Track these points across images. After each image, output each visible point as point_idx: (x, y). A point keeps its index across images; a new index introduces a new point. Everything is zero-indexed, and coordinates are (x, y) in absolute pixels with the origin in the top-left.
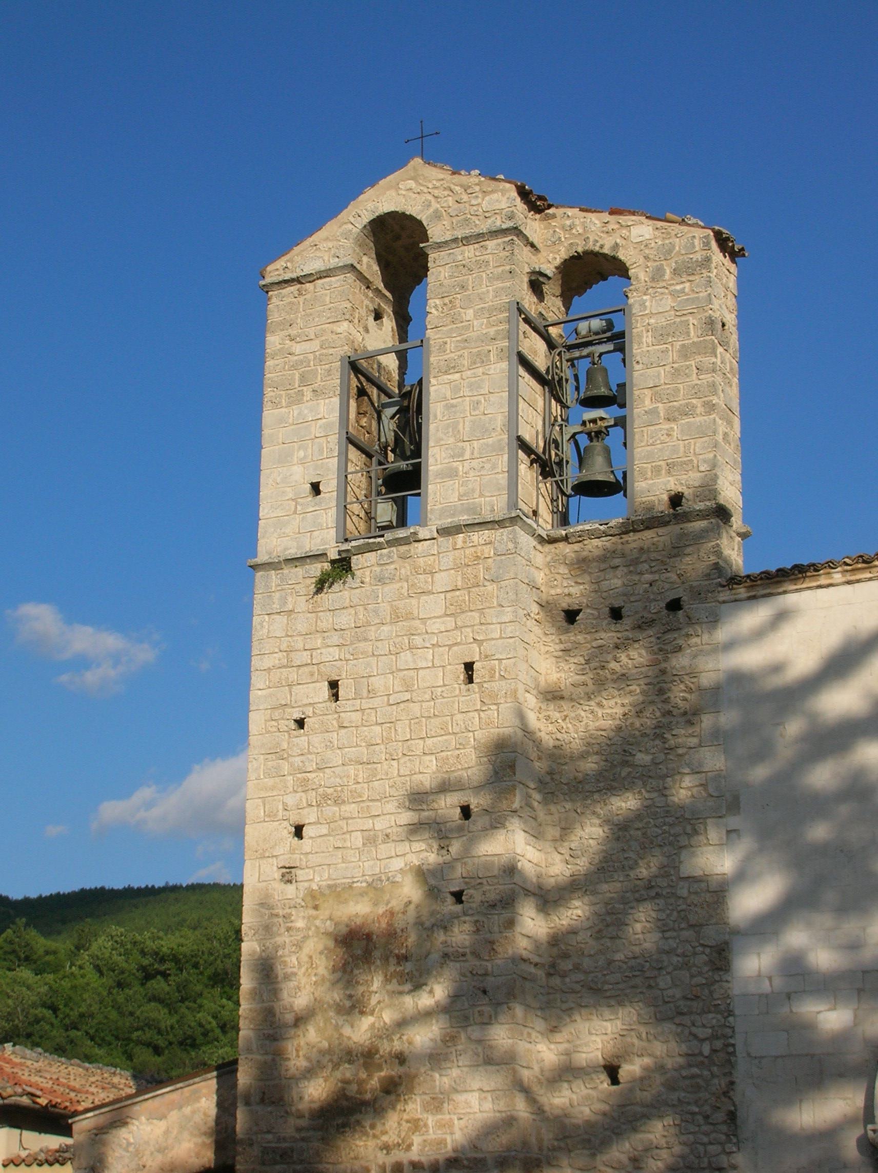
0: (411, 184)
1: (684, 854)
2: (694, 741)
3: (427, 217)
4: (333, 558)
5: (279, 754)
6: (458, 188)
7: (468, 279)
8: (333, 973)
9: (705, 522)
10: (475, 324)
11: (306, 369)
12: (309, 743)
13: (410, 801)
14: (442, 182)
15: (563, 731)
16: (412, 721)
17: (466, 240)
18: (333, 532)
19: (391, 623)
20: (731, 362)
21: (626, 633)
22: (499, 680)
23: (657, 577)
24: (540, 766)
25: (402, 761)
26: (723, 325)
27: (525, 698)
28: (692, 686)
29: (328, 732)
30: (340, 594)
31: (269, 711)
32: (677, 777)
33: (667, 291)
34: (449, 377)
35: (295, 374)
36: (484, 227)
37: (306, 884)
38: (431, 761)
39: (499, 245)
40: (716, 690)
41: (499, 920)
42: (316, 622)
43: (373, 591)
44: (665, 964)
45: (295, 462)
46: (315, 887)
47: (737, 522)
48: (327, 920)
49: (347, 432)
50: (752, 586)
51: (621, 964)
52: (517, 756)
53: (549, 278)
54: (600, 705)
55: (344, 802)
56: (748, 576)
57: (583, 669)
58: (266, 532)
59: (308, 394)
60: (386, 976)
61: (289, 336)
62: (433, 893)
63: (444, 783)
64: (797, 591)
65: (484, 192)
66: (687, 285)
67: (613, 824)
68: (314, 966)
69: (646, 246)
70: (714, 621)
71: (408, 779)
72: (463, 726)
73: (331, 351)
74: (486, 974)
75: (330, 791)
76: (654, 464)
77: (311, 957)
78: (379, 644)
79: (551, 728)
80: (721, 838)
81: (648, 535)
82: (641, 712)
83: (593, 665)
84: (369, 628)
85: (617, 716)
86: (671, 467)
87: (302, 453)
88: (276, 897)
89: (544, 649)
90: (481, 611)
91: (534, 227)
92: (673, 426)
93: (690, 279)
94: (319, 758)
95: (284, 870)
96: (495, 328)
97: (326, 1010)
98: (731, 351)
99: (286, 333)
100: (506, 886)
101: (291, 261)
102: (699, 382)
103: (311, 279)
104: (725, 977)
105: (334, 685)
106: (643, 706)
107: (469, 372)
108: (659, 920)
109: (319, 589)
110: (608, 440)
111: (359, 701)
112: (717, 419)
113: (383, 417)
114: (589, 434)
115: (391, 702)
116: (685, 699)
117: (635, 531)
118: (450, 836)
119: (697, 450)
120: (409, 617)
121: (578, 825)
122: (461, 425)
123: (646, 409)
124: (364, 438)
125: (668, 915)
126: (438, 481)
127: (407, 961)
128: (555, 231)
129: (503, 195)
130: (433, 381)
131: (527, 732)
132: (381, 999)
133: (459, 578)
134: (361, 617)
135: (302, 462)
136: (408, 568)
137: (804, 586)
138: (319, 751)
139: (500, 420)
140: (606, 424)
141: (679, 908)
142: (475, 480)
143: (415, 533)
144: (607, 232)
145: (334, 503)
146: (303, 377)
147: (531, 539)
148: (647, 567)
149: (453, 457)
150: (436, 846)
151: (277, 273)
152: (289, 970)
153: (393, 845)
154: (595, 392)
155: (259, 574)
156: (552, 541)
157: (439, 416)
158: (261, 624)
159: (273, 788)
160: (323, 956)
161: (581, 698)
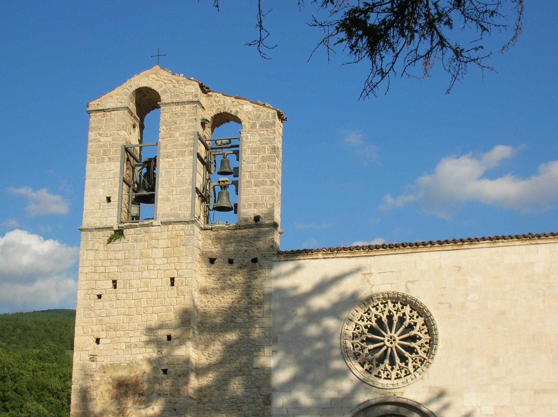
0: (154, 76)
1: (255, 359)
2: (261, 315)
3: (160, 92)
4: (116, 229)
5: (91, 309)
6: (174, 81)
7: (177, 120)
8: (111, 399)
9: (269, 228)
10: (180, 139)
11: (106, 148)
12: (103, 305)
13: (146, 332)
14: (167, 77)
15: (207, 307)
16: (148, 300)
17: (177, 103)
18: (116, 218)
19: (140, 258)
20: (279, 164)
21: (235, 270)
22: (185, 286)
23: (248, 248)
24: (199, 319)
25: (143, 315)
26: (278, 149)
27: (194, 293)
28: (261, 293)
29: (111, 301)
30: (118, 244)
31: (86, 290)
32: (253, 329)
33: (257, 133)
34: (168, 159)
35: (101, 150)
36: (186, 99)
37: (101, 363)
38: (155, 316)
39: (191, 107)
40: (270, 295)
41: (182, 381)
42: (108, 255)
43: (133, 245)
44: (246, 401)
45: (100, 187)
46: (104, 364)
47: (279, 229)
48: (109, 378)
49: (123, 177)
50: (286, 256)
51: (227, 400)
52: (191, 317)
53: (209, 122)
54: (223, 297)
55: (118, 330)
56: (285, 252)
57: (217, 283)
58: (86, 215)
59: (106, 158)
60: (134, 402)
61: (99, 133)
62: (155, 369)
63: (160, 325)
64: (304, 259)
65: (185, 84)
66: (266, 132)
67: (226, 345)
68: (103, 396)
69: (249, 113)
70: (271, 268)
71: (145, 323)
72: (169, 303)
73: (117, 142)
74: (176, 403)
75: (112, 325)
76: (249, 203)
77: (102, 392)
78: (135, 267)
79: (202, 305)
80: (270, 354)
81: (245, 231)
82: (240, 302)
83: (220, 281)
84: (130, 260)
85: (230, 302)
86: (256, 205)
87: (103, 184)
88: (88, 367)
89: (200, 273)
90: (178, 257)
91: (203, 99)
92: (257, 188)
93: (267, 130)
94: (107, 312)
95: (91, 356)
96: (188, 142)
97: (108, 414)
98: (280, 159)
99: (98, 132)
100: (185, 369)
101: (100, 101)
102: (268, 172)
103: (110, 111)
104: (269, 407)
105: (115, 282)
106: (240, 299)
107: (176, 159)
108: (244, 384)
109: (109, 241)
110: (228, 190)
111: (125, 289)
112: (275, 188)
113: (136, 170)
114: (221, 187)
115: (139, 291)
116: (257, 298)
117: (240, 229)
118: (163, 347)
119: (267, 199)
120: (148, 257)
121: (212, 345)
122: (172, 180)
123: (247, 180)
124: (128, 179)
125: (247, 382)
126: (162, 202)
127: (143, 396)
128: (211, 102)
129: (193, 86)
130: (161, 160)
131: (195, 307)
132: (132, 411)
133: (170, 243)
134: (127, 255)
135: (103, 187)
136: (148, 236)
137: (307, 258)
138: (108, 308)
139: (189, 180)
140: (228, 183)
141: (252, 380)
142: (178, 204)
143: (152, 223)
144: (234, 106)
145: (117, 206)
146: (104, 152)
147: (198, 229)
148: (244, 244)
149: (168, 193)
150: (156, 351)
151: (94, 106)
152: (92, 397)
153: (138, 349)
154: (225, 170)
155: (83, 233)
156: (205, 229)
157: (163, 175)
158: (83, 254)
159: (87, 322)
160: (107, 392)
161: (215, 294)
